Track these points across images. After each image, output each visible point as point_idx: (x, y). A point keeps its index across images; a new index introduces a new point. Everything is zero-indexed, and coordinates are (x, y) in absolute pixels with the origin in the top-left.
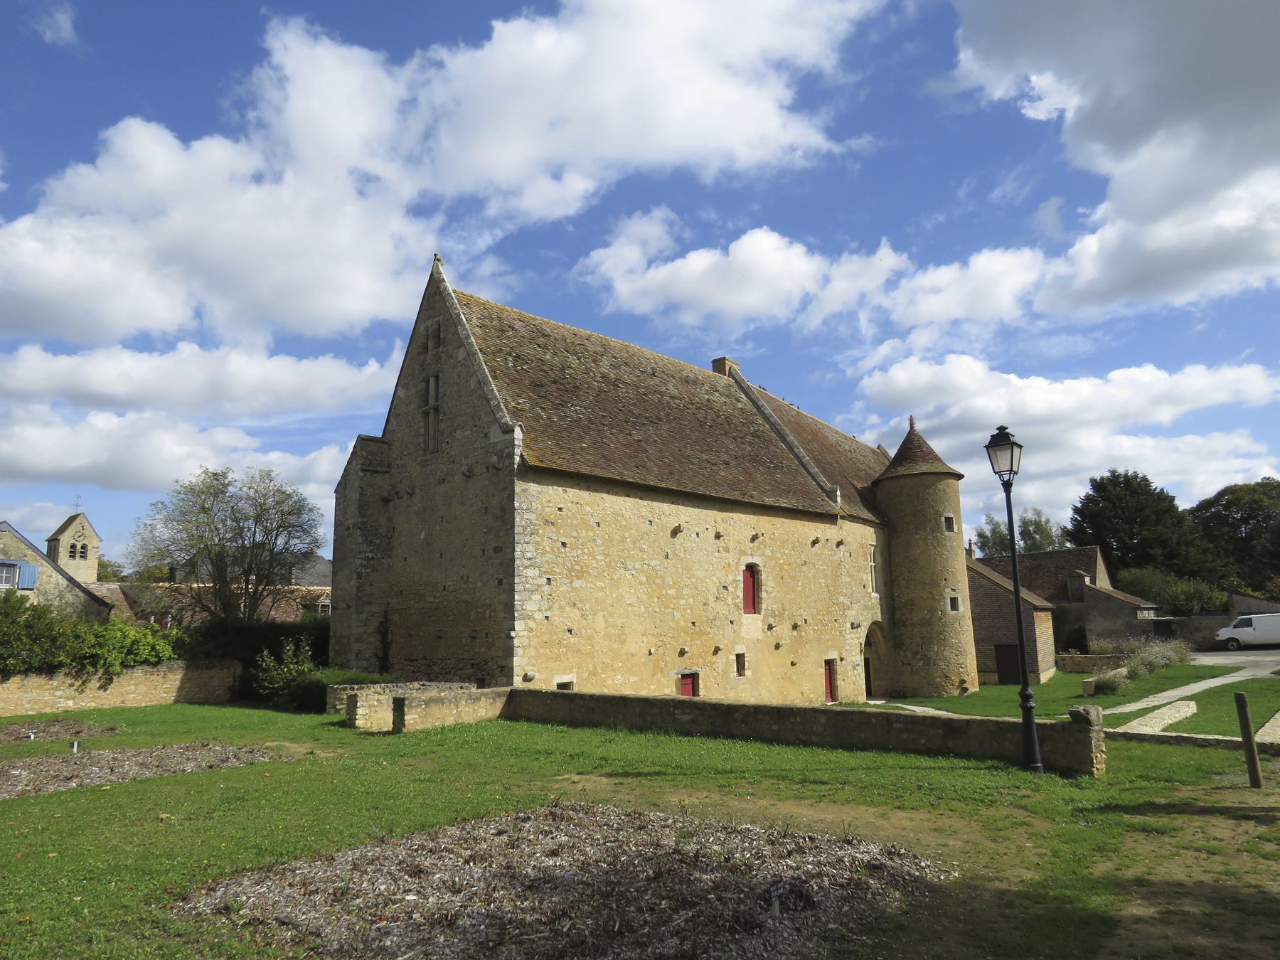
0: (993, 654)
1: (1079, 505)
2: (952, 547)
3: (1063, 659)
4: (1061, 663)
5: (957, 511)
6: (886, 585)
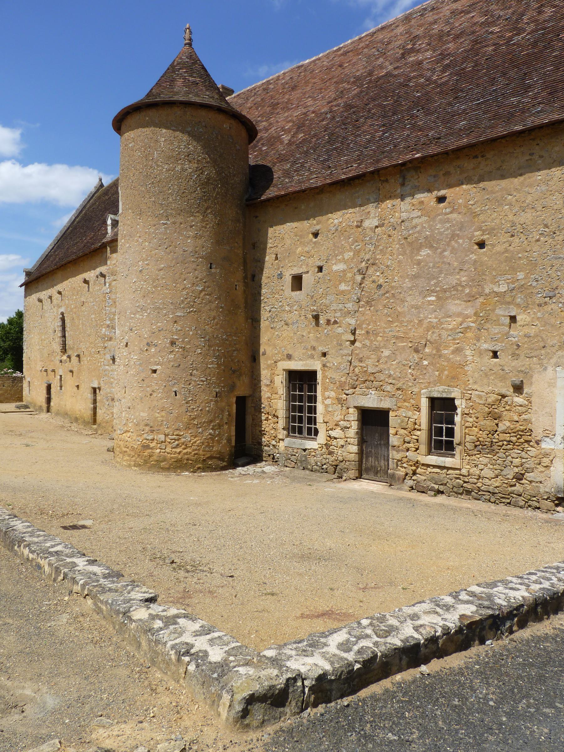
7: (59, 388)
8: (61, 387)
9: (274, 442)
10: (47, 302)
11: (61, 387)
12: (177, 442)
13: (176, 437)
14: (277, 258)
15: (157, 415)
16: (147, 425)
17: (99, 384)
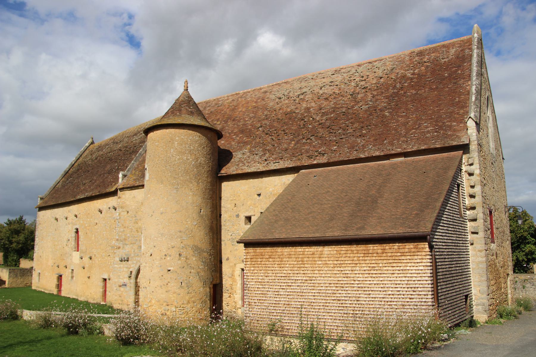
7: (70, 278)
8: (72, 277)
9: (234, 310)
10: (62, 222)
11: (72, 277)
12: (182, 311)
13: (182, 309)
14: (235, 206)
15: (171, 296)
16: (165, 302)
17: (109, 276)
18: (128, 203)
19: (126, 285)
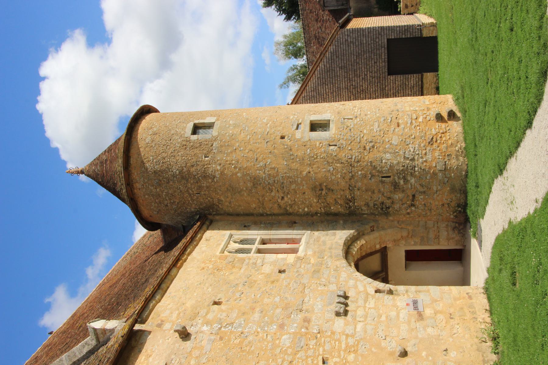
0: (399, 78)
1: (284, 16)
2: (235, 126)
3: (406, 6)
4: (411, 10)
5: (183, 117)
6: (133, 348)
18: (189, 304)
19: (415, 302)
